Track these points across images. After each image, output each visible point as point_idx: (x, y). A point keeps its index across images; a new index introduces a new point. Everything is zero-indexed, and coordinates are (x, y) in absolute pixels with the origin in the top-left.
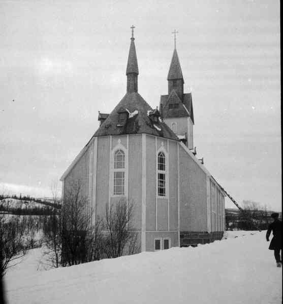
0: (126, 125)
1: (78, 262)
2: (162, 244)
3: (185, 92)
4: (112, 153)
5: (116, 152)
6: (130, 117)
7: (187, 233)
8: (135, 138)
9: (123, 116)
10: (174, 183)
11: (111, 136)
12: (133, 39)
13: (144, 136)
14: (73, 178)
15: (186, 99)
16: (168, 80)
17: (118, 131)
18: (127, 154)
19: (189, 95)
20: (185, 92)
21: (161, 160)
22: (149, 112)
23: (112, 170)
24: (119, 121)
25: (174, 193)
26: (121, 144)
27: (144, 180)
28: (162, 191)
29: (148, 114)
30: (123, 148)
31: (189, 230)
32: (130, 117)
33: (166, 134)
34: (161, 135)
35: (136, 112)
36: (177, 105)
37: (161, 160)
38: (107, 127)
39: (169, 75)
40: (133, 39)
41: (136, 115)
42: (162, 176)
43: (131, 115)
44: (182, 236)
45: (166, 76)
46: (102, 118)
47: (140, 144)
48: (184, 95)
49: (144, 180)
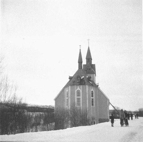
0: (80, 82)
1: (9, 133)
2: (93, 123)
3: (93, 63)
4: (76, 91)
5: (77, 91)
6: (81, 78)
7: (101, 119)
8: (84, 86)
9: (79, 78)
10: (96, 102)
11: (75, 86)
12: (80, 50)
13: (87, 86)
14: (59, 98)
15: (93, 67)
16: (86, 59)
17: (78, 84)
18: (81, 91)
19: (94, 65)
20: (93, 63)
21: (92, 94)
22: (87, 76)
23: (81, 97)
24: (78, 80)
25: (96, 104)
26: (79, 88)
27: (87, 101)
28: (93, 104)
29: (87, 77)
30: (80, 90)
31: (101, 118)
32: (81, 78)
33: (94, 85)
34: (92, 85)
35: (83, 77)
36: (90, 69)
37: (92, 94)
38: (74, 82)
39: (86, 57)
40: (80, 50)
41: (83, 78)
42: (93, 99)
43: (82, 78)
44: (99, 120)
45: (85, 58)
46: (71, 78)
47: (86, 88)
48: (92, 65)
49: (87, 101)
